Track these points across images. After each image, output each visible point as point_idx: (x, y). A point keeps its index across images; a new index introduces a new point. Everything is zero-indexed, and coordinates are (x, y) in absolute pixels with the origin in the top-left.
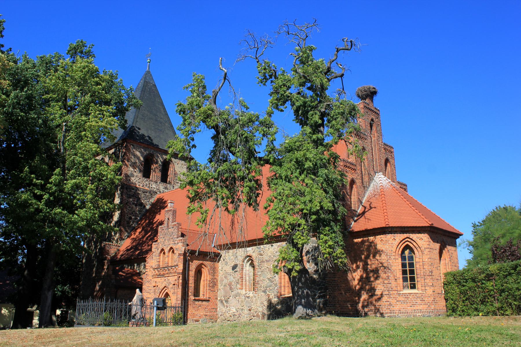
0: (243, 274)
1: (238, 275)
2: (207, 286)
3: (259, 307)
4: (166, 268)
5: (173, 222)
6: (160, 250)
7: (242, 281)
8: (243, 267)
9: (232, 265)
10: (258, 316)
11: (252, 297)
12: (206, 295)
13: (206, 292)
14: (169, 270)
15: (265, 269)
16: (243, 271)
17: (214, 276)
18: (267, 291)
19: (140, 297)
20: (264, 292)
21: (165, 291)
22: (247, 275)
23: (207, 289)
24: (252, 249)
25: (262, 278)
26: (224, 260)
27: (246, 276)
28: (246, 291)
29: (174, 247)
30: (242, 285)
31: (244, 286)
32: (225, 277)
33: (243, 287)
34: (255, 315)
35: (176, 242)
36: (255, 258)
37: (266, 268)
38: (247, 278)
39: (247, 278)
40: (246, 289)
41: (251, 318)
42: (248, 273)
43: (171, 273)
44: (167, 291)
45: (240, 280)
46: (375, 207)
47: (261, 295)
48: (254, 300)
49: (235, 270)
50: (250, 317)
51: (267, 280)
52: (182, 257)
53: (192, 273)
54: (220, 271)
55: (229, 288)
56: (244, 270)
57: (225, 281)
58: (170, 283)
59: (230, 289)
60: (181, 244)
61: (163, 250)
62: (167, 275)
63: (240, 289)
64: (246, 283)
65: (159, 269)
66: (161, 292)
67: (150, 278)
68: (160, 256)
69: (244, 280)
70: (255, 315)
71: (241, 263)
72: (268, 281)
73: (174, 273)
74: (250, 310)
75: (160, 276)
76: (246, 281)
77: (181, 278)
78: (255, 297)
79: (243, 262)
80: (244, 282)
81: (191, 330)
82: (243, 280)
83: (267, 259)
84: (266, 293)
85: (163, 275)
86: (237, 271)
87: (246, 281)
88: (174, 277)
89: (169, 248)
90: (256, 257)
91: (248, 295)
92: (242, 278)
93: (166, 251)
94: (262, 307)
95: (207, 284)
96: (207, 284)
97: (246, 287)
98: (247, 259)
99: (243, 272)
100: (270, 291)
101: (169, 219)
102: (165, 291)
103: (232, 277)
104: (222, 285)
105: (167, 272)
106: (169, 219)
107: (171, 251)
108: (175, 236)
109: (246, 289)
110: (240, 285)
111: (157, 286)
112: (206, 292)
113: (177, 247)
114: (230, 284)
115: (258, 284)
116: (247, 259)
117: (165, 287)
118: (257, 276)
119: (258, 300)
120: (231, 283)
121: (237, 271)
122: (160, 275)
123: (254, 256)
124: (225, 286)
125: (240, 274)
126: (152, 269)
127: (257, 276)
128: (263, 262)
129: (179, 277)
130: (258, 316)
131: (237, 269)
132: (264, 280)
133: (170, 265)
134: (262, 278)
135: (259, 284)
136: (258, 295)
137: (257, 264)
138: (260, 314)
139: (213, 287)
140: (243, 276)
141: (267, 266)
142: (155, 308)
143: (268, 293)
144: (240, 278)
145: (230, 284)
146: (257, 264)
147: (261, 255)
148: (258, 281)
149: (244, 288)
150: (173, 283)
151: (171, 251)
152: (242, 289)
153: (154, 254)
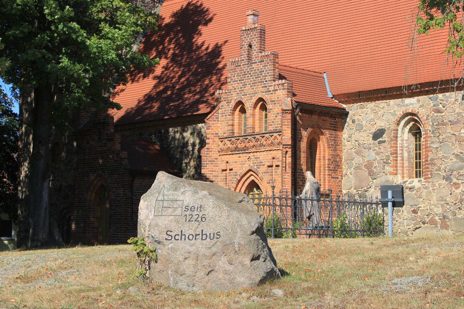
0: (397, 147)
1: (386, 149)
2: (324, 170)
3: (436, 206)
4: (249, 137)
5: (262, 50)
6: (233, 103)
7: (397, 160)
8: (397, 134)
9: (373, 130)
10: (433, 222)
11: (419, 188)
12: (324, 185)
13: (324, 180)
14: (257, 140)
15: (448, 137)
16: (397, 141)
17: (335, 150)
18: (452, 177)
19: (316, 186)
20: (447, 178)
21: (248, 178)
22: (405, 149)
23: (324, 175)
24: (419, 101)
25: (440, 154)
26: (353, 121)
27: (402, 150)
28: (403, 177)
29: (266, 97)
30: (396, 167)
31: (399, 168)
32: (358, 153)
33: (397, 170)
34: (427, 220)
35: (271, 89)
36: (425, 118)
37: (449, 135)
38: (406, 155)
39: (406, 155)
40: (403, 174)
41: (418, 226)
42: (405, 145)
43: (262, 145)
44: (252, 178)
45: (391, 159)
46: (226, 42)
47: (440, 185)
48: (424, 194)
49: (381, 139)
50: (415, 224)
51: (452, 157)
52: (289, 116)
53: (303, 145)
54: (345, 142)
55: (367, 173)
56: (399, 139)
57: (358, 160)
58: (261, 164)
59: (369, 174)
60: (285, 92)
61: (240, 103)
62: (254, 150)
63: (391, 173)
64: (403, 164)
65: (233, 139)
66: (239, 181)
67: (214, 154)
68: (233, 114)
69: (399, 158)
70: (427, 220)
71: (393, 127)
72: (454, 160)
73: (269, 145)
74: (415, 212)
75: (236, 150)
76: (402, 160)
77: (289, 154)
78: (426, 188)
79: (398, 124)
80: (399, 162)
81: (358, 247)
82: (397, 157)
83: (452, 118)
84: (451, 180)
85: (245, 150)
86: (384, 142)
87: (402, 160)
88: (269, 152)
89: (254, 100)
90: (428, 116)
91: (410, 186)
92: (396, 153)
93: (248, 105)
94: (442, 205)
95: (324, 165)
96: (324, 165)
97: (403, 170)
98: (407, 118)
99: (396, 144)
100: (460, 178)
101: (250, 46)
102: (248, 178)
103: (373, 154)
104: (350, 167)
105: (251, 144)
106: (250, 46)
107: (239, 108)
108: (269, 78)
109: (403, 174)
110: (392, 167)
111: (231, 170)
112: (324, 180)
113: (274, 97)
114: (369, 166)
115: (431, 164)
116: (407, 118)
117: (250, 170)
118: (431, 151)
119: (434, 194)
120: (372, 163)
121: (384, 142)
122: (236, 149)
123: (422, 113)
124: (357, 168)
125: (391, 147)
126: (217, 139)
127: (431, 151)
128: (443, 124)
129: (287, 152)
130: (433, 222)
131: (385, 137)
132: (445, 157)
133: (257, 130)
134: (440, 154)
135: (435, 164)
136: (434, 185)
137: (430, 128)
138: (437, 218)
139: (335, 171)
140: (397, 150)
141: (452, 132)
142: (390, 204)
143: (455, 180)
144: (391, 154)
145: (369, 166)
146: (430, 128)
147: (439, 111)
148: (432, 160)
149: (400, 172)
150: (269, 164)
151: (239, 108)
152: (396, 174)
153: (220, 111)
